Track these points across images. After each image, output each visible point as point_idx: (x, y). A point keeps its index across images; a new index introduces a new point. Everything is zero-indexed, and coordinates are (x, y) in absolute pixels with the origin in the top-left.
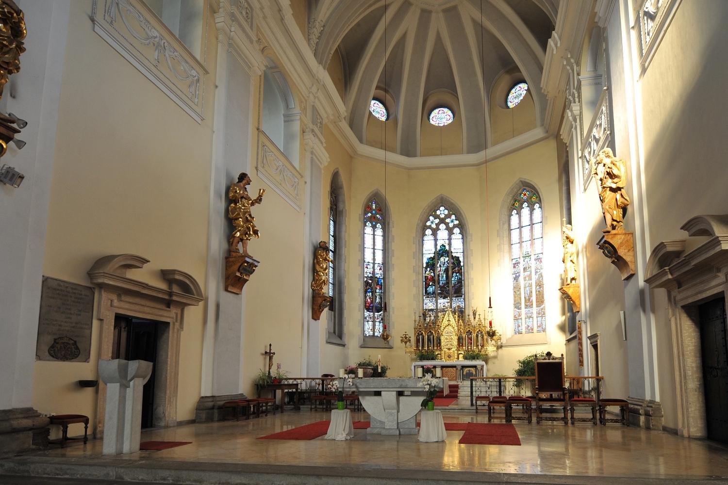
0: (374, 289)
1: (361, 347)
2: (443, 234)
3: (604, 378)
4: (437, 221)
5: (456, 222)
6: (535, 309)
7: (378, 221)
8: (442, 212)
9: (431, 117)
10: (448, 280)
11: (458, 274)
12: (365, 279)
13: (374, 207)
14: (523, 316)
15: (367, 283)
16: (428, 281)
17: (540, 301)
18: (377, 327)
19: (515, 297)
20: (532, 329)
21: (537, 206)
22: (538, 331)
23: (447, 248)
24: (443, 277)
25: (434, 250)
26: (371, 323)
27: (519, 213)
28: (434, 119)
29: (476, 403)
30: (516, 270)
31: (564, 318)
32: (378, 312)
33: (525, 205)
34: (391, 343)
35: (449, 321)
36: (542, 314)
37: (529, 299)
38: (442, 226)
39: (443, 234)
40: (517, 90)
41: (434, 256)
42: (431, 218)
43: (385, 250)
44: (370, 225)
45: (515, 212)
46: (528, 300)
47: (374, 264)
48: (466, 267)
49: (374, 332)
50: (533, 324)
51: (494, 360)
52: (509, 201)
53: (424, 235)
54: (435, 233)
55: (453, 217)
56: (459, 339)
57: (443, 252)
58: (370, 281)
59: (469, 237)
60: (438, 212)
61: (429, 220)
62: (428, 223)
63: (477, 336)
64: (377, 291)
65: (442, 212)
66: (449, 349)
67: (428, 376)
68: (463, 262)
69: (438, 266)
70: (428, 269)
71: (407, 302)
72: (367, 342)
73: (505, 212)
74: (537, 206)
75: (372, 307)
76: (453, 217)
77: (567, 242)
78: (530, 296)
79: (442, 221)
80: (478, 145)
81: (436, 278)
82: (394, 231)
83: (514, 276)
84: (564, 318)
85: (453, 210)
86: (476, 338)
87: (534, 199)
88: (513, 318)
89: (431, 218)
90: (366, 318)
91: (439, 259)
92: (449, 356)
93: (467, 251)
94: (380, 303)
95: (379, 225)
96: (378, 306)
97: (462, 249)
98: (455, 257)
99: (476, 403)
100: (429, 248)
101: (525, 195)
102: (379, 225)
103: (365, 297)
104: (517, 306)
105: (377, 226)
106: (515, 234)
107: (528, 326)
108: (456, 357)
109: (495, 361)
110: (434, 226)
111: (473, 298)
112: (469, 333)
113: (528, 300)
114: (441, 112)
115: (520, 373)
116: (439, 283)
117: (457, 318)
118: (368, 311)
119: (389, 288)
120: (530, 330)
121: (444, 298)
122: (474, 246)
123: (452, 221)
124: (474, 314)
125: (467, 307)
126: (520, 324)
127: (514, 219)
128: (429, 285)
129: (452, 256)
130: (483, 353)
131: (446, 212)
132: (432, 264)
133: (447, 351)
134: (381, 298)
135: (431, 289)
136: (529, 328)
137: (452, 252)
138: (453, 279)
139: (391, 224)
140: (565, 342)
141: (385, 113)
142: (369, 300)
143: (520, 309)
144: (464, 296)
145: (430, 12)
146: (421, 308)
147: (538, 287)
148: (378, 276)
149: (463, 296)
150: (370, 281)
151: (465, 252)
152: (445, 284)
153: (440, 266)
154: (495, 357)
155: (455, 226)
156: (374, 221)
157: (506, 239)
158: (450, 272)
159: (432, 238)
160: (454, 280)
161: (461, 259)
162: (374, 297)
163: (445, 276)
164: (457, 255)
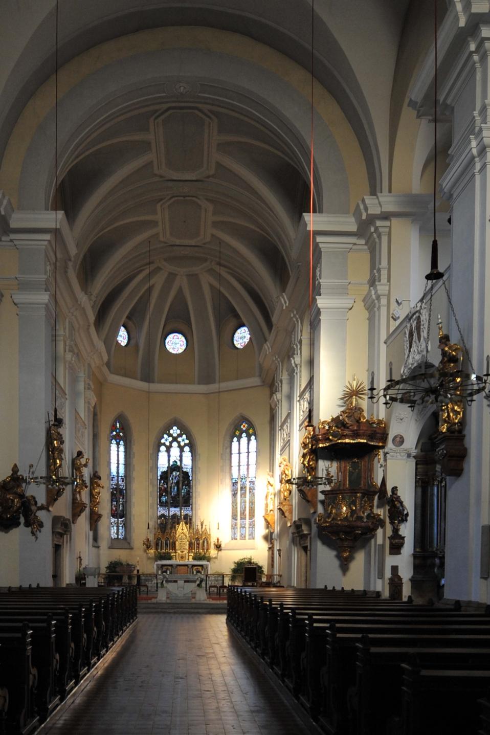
0: (118, 499)
1: (110, 548)
2: (175, 451)
3: (283, 575)
4: (170, 439)
5: (187, 441)
6: (247, 521)
7: (121, 439)
8: (175, 431)
9: (166, 341)
10: (178, 490)
11: (187, 487)
12: (111, 490)
13: (118, 425)
14: (239, 526)
15: (112, 494)
16: (163, 492)
17: (252, 515)
18: (120, 531)
19: (233, 510)
20: (245, 537)
21: (253, 438)
22: (249, 539)
23: (179, 463)
24: (174, 489)
25: (167, 465)
26: (115, 528)
27: (239, 441)
28: (169, 343)
29: (210, 590)
30: (234, 487)
31: (267, 531)
32: (121, 518)
33: (244, 435)
34: (132, 544)
35: (182, 530)
36: (252, 525)
37: (244, 513)
39: (175, 451)
40: (242, 332)
41: (167, 470)
42: (165, 436)
43: (126, 465)
44: (115, 442)
45: (235, 439)
46: (243, 513)
47: (118, 476)
48: (194, 481)
49: (118, 535)
50: (245, 533)
51: (214, 560)
52: (231, 430)
53: (159, 451)
54: (168, 449)
55: (184, 436)
56: (190, 545)
57: (174, 468)
58: (115, 492)
59: (197, 457)
60: (171, 432)
61: (163, 438)
62: (163, 441)
63: (204, 542)
64: (121, 500)
65: (175, 431)
66: (182, 552)
67: (199, 574)
68: (192, 477)
69: (171, 479)
70: (162, 481)
71: (145, 509)
72: (115, 544)
73: (228, 439)
74: (253, 438)
75: (117, 514)
76: (184, 436)
77: (269, 485)
78: (245, 510)
79: (175, 439)
80: (207, 378)
81: (169, 489)
82: (135, 448)
83: (233, 492)
84: (267, 531)
85: (184, 430)
86: (199, 542)
87: (251, 431)
88: (231, 527)
89: (165, 436)
90: (112, 524)
91: (172, 473)
92: (182, 557)
93: (195, 468)
94: (123, 511)
95: (122, 442)
96: (121, 513)
97: (191, 466)
98: (185, 472)
99: (210, 590)
100: (163, 463)
101: (244, 426)
102: (122, 442)
103: (112, 506)
104: (234, 517)
105: (121, 443)
106: (235, 458)
107: (242, 534)
108: (187, 558)
109: (216, 560)
110: (168, 444)
111: (199, 509)
112: (198, 539)
113: (243, 513)
114: (176, 337)
115: (235, 571)
116: (171, 494)
117: (188, 528)
118: (113, 517)
119: (130, 498)
120: (243, 537)
121: (175, 507)
122: (201, 464)
123: (183, 440)
124: (202, 525)
125: (194, 515)
126: (236, 532)
127: (235, 444)
128: (163, 495)
129: (183, 471)
130: (207, 555)
131: (179, 432)
132: (165, 476)
133: (180, 553)
134: (123, 506)
135: (164, 499)
136: (243, 536)
137: (182, 468)
138: (183, 491)
139: (132, 442)
140: (267, 549)
141: (127, 336)
142: (114, 508)
143: (236, 520)
144: (192, 506)
145: (176, 275)
146: (156, 515)
147: (251, 504)
148: (121, 487)
149: (191, 506)
150: (115, 492)
151: (194, 469)
152: (175, 495)
153: (172, 479)
154: (216, 558)
155: (186, 445)
156: (117, 438)
157: (228, 462)
158: (181, 485)
159: (166, 454)
160: (183, 492)
162: (117, 506)
163: (176, 488)
164: (188, 470)
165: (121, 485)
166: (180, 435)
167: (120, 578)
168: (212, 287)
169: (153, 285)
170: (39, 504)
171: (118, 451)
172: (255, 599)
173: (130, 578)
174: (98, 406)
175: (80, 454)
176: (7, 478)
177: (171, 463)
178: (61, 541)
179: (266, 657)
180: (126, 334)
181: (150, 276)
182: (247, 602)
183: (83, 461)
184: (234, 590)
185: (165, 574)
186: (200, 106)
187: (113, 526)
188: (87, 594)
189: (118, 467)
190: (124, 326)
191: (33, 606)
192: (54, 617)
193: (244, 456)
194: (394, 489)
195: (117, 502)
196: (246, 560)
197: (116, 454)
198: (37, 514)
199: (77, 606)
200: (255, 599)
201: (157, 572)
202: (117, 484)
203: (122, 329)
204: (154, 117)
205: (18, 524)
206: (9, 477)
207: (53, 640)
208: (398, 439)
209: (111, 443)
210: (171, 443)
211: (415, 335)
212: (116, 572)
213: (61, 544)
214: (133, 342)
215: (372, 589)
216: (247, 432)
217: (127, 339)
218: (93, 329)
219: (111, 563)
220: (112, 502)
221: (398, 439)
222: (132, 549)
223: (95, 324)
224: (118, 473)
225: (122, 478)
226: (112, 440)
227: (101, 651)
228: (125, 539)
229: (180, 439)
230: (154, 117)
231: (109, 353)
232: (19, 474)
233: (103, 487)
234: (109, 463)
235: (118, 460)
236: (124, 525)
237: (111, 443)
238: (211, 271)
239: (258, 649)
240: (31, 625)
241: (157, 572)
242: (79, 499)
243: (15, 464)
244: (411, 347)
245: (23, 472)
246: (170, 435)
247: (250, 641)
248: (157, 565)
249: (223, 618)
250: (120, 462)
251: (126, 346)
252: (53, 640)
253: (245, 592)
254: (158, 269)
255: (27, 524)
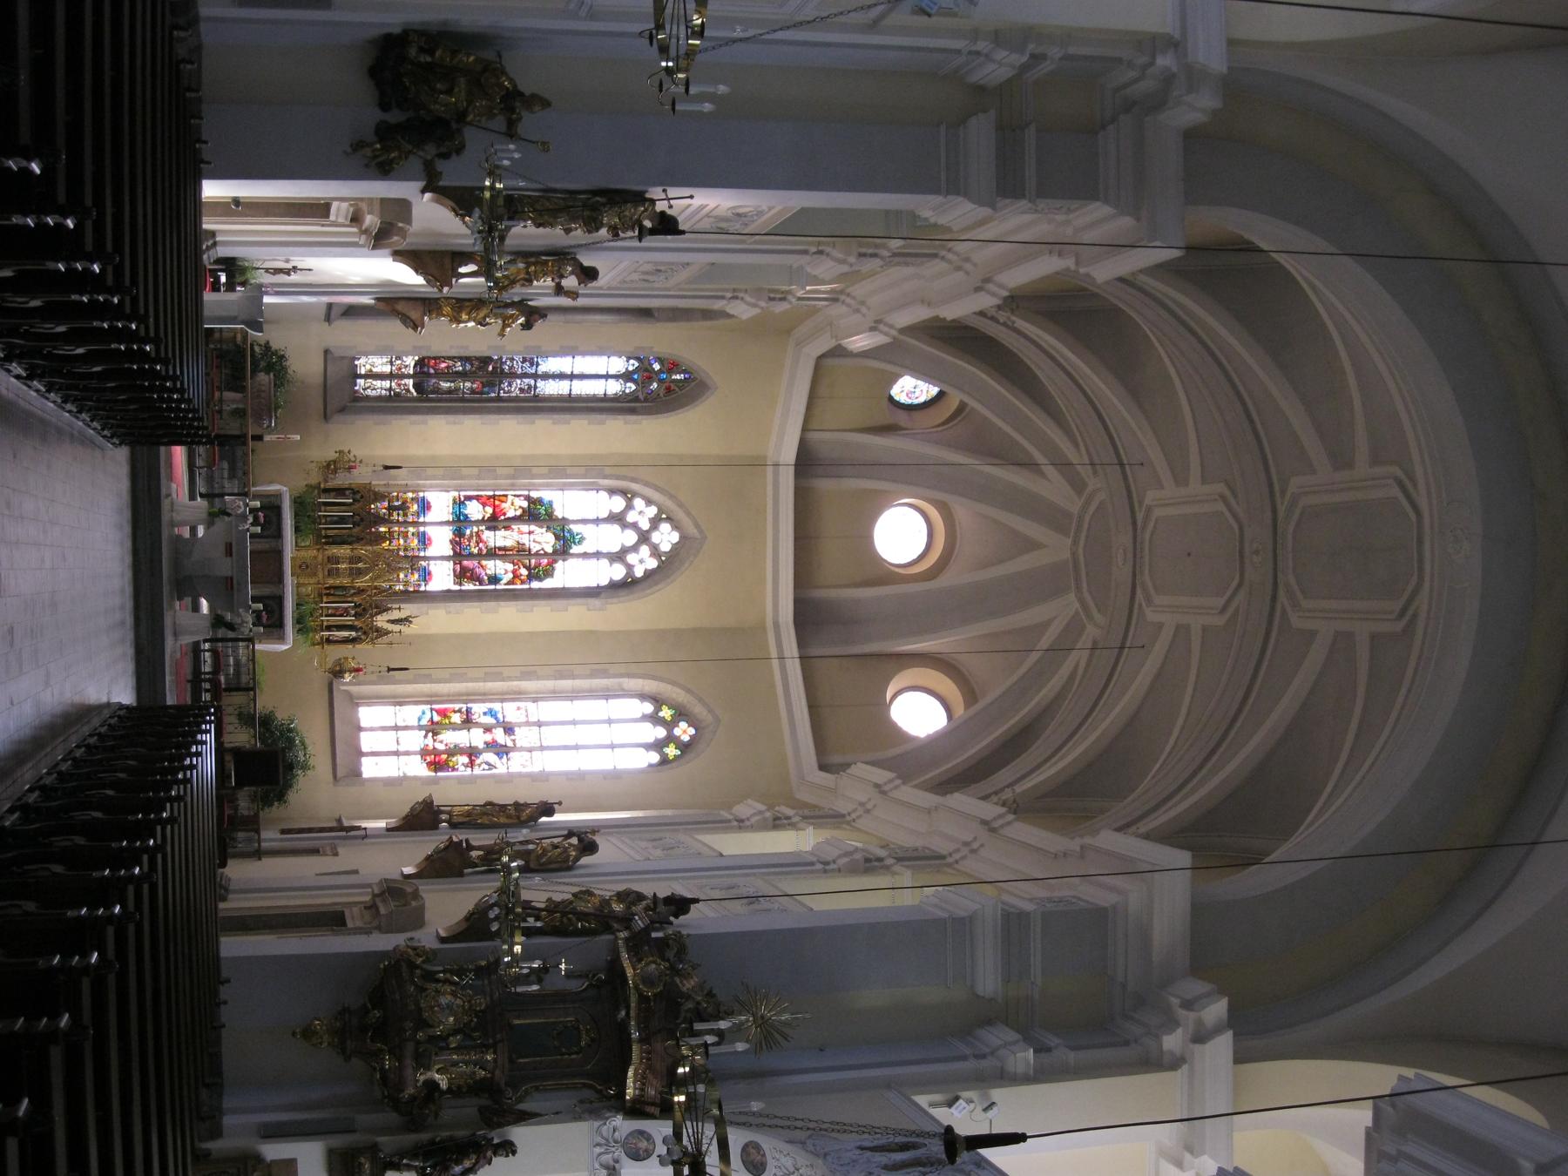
4: (645, 525)
15: (486, 360)
18: (378, 383)
21: (654, 757)
26: (387, 369)
27: (645, 718)
33: (661, 732)
38: (631, 538)
47: (535, 376)
49: (366, 377)
54: (617, 519)
60: (665, 527)
64: (468, 384)
65: (666, 537)
74: (654, 757)
79: (644, 538)
85: (669, 564)
87: (672, 751)
90: (398, 358)
94: (437, 390)
95: (631, 387)
100: (570, 503)
102: (631, 387)
132: (535, 513)
134: (450, 391)
141: (916, 402)
155: (630, 567)
156: (643, 374)
161: (548, 584)
165: (510, 385)
166: (655, 551)
167: (236, 382)
168: (1044, 626)
169: (1042, 474)
170: (441, 165)
171: (607, 377)
172: (178, 782)
173: (240, 413)
174: (728, 321)
175: (589, 274)
176: (511, 80)
177: (575, 528)
178: (341, 220)
179: (16, 815)
180: (922, 400)
181: (1064, 466)
182: (171, 759)
183: (570, 282)
184: (206, 722)
185: (251, 520)
186: (1427, 585)
187: (391, 363)
188: (181, 335)
189: (561, 376)
190: (941, 395)
191: (139, 62)
192: (110, 269)
193: (603, 734)
194: (508, 1148)
195: (463, 375)
196: (301, 754)
197: (598, 370)
198: (411, 157)
199: (142, 311)
200: (178, 782)
201: (256, 497)
202: (513, 375)
203: (934, 391)
204: (1403, 477)
205: (384, 106)
206: (515, 86)
207: (50, 265)
208: (643, 1144)
209: (629, 359)
210: (634, 526)
211: (899, 1157)
212: (254, 372)
213: (332, 218)
214: (902, 418)
215: (227, 1103)
216: (671, 738)
217: (909, 402)
218: (920, 314)
219: (283, 356)
220: (461, 359)
221: (643, 1144)
222: (326, 417)
223: (937, 318)
224: (546, 376)
225: (530, 387)
226: (638, 359)
227: (19, 364)
228: (357, 398)
229: (645, 550)
230: (1403, 477)
231: (865, 354)
232: (525, 114)
233: (502, 334)
234: (572, 351)
235: (582, 377)
236: (398, 395)
237: (629, 359)
238: (1073, 628)
239: (37, 793)
240: (89, 225)
241: (256, 497)
242: (462, 270)
243: (546, 104)
244: (874, 1149)
245: (530, 123)
246: (655, 523)
247: (60, 773)
248: (278, 496)
249: (125, 696)
250: (576, 383)
251: (891, 399)
252: (50, 265)
253: (198, 754)
254: (1078, 486)
255: (385, 133)
